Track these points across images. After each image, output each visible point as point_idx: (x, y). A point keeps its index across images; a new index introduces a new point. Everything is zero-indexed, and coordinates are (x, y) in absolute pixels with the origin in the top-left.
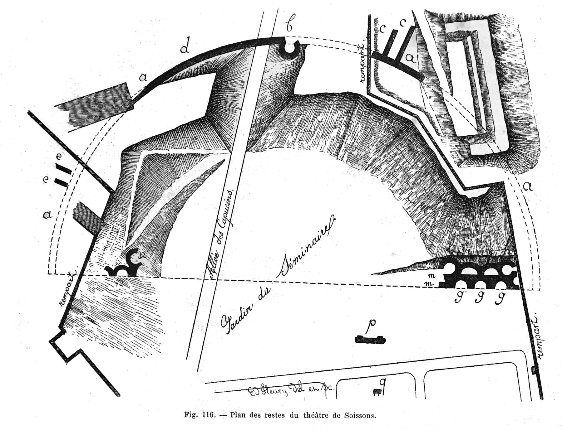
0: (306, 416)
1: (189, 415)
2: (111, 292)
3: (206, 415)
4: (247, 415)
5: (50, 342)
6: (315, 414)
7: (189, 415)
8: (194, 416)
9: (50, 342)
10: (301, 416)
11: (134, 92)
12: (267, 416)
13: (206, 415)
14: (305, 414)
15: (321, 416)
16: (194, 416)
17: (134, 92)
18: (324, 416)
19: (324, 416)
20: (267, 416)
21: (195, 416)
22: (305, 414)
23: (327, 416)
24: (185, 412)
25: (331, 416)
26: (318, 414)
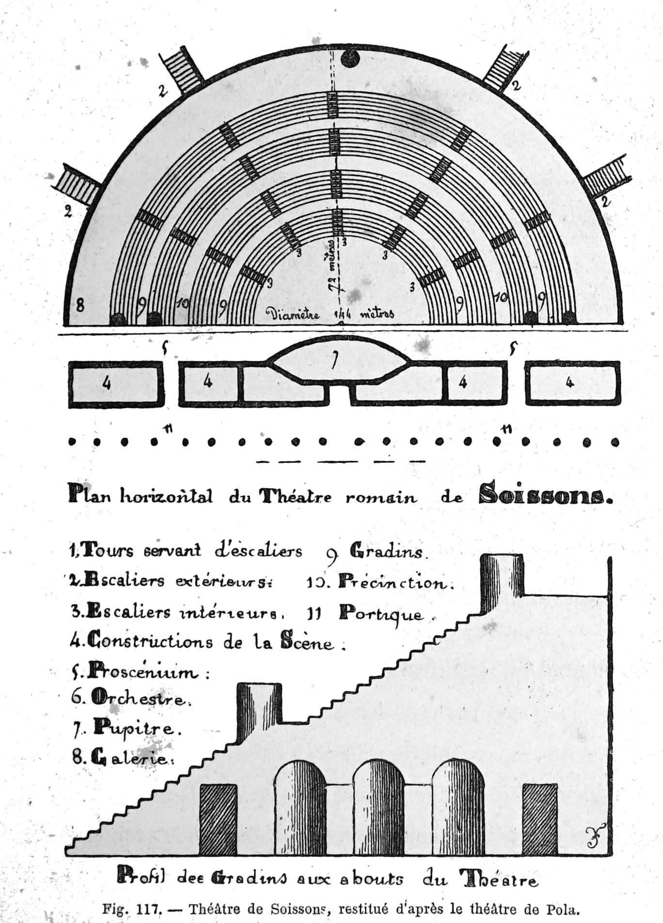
0: (475, 911)
1: (112, 910)
2: (514, 258)
3: (144, 910)
4: (244, 910)
5: (619, 363)
6: (490, 906)
7: (112, 910)
8: (120, 912)
9: (619, 363)
10: (467, 910)
11: (339, 53)
12: (344, 910)
13: (144, 910)
14: (472, 907)
15: (503, 910)
16: (119, 912)
17: (339, 53)
18: (508, 911)
19: (508, 911)
20: (344, 910)
21: (124, 911)
22: (472, 907)
23: (513, 910)
24: (105, 905)
25: (244, 910)
26: (221, 906)
